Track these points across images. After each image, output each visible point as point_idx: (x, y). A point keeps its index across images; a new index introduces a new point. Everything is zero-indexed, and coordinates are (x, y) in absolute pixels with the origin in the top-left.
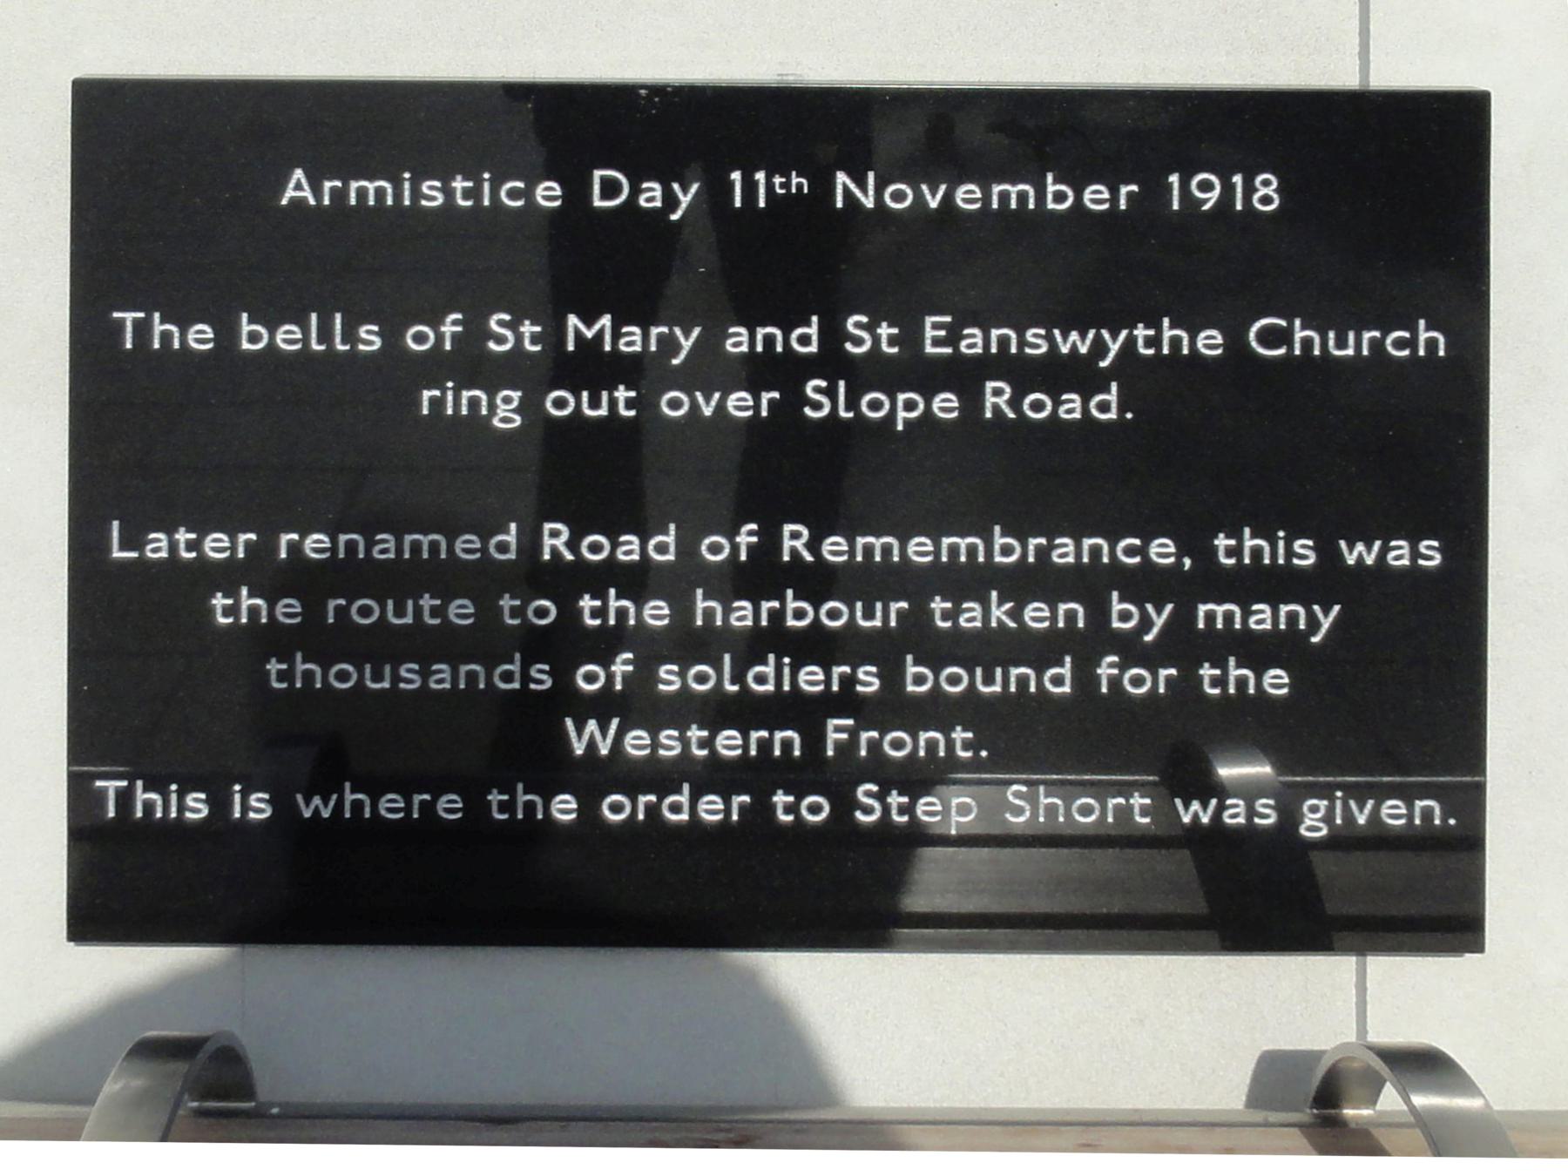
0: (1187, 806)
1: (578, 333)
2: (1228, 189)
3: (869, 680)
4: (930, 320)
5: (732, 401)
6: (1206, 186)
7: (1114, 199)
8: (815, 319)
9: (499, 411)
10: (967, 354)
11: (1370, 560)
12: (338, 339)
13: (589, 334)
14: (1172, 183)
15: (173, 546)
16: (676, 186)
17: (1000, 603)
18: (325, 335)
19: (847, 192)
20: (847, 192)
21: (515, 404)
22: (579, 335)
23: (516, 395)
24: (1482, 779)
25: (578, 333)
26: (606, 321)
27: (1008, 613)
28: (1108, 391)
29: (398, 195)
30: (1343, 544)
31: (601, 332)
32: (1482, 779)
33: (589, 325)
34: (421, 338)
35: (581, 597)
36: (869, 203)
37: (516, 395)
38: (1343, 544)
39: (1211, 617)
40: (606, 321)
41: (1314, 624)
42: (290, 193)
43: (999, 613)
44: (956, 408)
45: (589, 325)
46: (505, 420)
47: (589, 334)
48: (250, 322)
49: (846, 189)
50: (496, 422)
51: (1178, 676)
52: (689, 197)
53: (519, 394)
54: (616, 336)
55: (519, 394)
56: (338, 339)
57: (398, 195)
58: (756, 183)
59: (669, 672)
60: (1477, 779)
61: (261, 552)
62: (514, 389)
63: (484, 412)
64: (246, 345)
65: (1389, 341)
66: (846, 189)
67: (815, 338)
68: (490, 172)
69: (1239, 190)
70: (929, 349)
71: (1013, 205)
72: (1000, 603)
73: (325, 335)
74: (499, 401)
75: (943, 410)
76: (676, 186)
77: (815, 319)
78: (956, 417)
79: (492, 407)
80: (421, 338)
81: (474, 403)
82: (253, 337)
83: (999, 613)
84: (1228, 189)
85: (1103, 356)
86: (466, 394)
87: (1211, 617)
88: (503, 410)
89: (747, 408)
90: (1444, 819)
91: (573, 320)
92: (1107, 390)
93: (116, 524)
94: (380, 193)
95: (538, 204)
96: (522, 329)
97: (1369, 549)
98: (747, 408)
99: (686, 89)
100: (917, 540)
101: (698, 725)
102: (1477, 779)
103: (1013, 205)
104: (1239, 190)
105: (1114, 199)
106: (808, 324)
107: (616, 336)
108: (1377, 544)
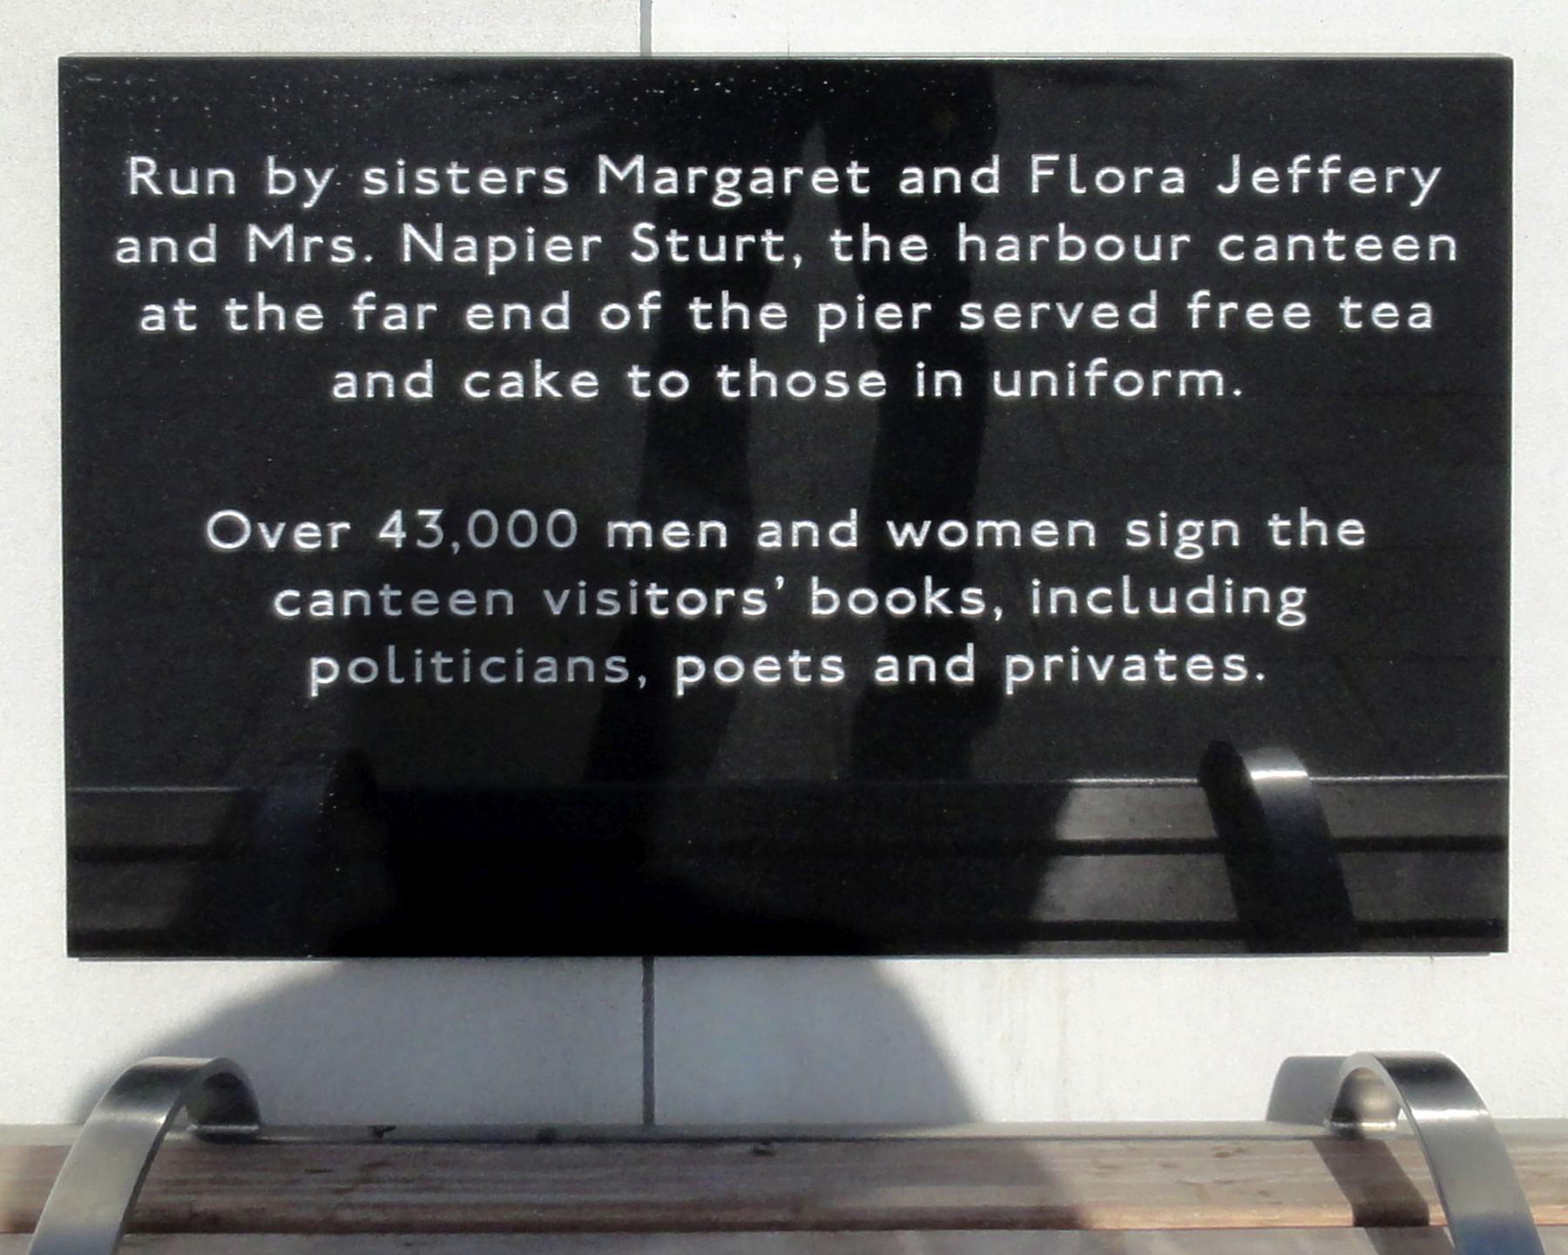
0: (899, 529)
1: (259, 242)
4: (1036, 159)
5: (905, 246)
8: (854, 512)
13: (271, 245)
17: (544, 372)
19: (415, 246)
20: (415, 246)
24: (1505, 777)
25: (259, 242)
26: (638, 162)
27: (551, 382)
28: (827, 332)
31: (633, 175)
32: (1505, 777)
33: (621, 167)
36: (437, 256)
40: (638, 162)
43: (543, 383)
44: (1276, 183)
45: (621, 167)
47: (271, 245)
48: (759, 369)
49: (414, 243)
54: (650, 178)
60: (1498, 777)
61: (361, 542)
63: (1266, 610)
64: (816, 611)
65: (1117, 381)
66: (414, 243)
67: (854, 532)
68: (405, 159)
71: (999, 543)
75: (1263, 185)
77: (854, 512)
78: (1379, 260)
79: (1276, 605)
82: (825, 602)
83: (543, 383)
85: (307, 197)
87: (620, 535)
88: (1287, 608)
90: (1229, 387)
91: (604, 162)
92: (828, 334)
95: (549, 259)
96: (849, 171)
100: (1293, 306)
102: (1498, 777)
103: (999, 543)
106: (847, 518)
107: (650, 178)
108: (927, 525)
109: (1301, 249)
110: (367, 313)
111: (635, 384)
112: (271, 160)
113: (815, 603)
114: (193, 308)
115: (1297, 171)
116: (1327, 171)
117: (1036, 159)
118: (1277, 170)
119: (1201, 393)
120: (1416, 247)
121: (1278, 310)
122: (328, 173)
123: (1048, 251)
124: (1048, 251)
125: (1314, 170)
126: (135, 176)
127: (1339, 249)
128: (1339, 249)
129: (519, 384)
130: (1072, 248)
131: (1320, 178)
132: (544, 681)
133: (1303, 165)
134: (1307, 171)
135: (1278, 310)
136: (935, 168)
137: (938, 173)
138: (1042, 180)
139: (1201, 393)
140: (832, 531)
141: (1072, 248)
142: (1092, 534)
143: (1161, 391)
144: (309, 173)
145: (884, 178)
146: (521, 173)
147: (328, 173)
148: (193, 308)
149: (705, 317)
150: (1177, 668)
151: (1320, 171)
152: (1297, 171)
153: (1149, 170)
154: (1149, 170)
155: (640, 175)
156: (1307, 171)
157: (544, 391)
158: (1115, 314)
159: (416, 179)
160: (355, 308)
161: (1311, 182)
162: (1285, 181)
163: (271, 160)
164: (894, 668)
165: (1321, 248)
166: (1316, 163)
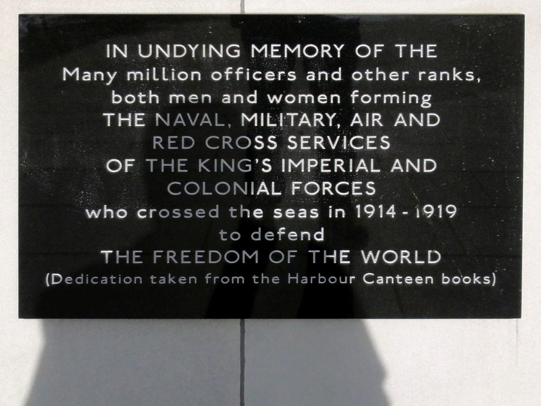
1: (67, 74)
2: (377, 211)
3: (292, 76)
4: (155, 252)
6: (369, 209)
7: (276, 76)
9: (423, 102)
10: (431, 81)
11: (278, 101)
12: (164, 76)
14: (357, 209)
15: (109, 280)
16: (108, 73)
17: (457, 72)
18: (159, 75)
21: (429, 100)
22: (67, 75)
23: (429, 96)
26: (77, 70)
29: (145, 76)
30: (269, 96)
34: (217, 76)
35: (220, 231)
37: (429, 96)
38: (269, 96)
39: (132, 76)
40: (77, 70)
41: (107, 79)
42: (394, 168)
46: (425, 105)
50: (422, 106)
51: (355, 278)
52: (113, 77)
53: (430, 96)
54: (81, 75)
55: (430, 96)
56: (164, 76)
57: (145, 76)
58: (439, 209)
59: (487, 278)
62: (429, 94)
63: (417, 102)
69: (381, 211)
70: (129, 73)
72: (457, 72)
73: (159, 75)
74: (423, 98)
76: (108, 73)
79: (421, 101)
80: (217, 76)
81: (414, 99)
84: (377, 211)
86: (411, 96)
87: (132, 76)
88: (424, 102)
89: (273, 77)
91: (65, 70)
93: (152, 170)
94: (138, 76)
97: (278, 98)
98: (273, 77)
99: (131, 77)
101: (138, 94)
104: (381, 211)
105: (276, 76)
107: (81, 75)
109: (390, 280)
110: (209, 279)
111: (255, 280)
112: (443, 274)
113: (319, 280)
114: (155, 277)
115: (227, 73)
116: (238, 73)
117: (155, 252)
118: (294, 210)
119: (238, 282)
120: (422, 280)
121: (414, 278)
122: (115, 73)
123: (316, 281)
124: (316, 281)
125: (234, 73)
126: (155, 143)
127: (400, 280)
128: (400, 280)
129: (164, 280)
130: (322, 280)
131: (235, 75)
132: (162, 283)
133: (230, 70)
134: (231, 73)
135: (414, 278)
136: (410, 113)
137: (236, 96)
138: (157, 259)
139: (238, 282)
140: (228, 281)
141: (322, 280)
142: (432, 280)
143: (313, 282)
144: (190, 46)
145: (351, 211)
146: (280, 73)
147: (115, 73)
148: (155, 277)
149: (257, 280)
150: (402, 280)
151: (236, 73)
152: (227, 73)
153: (424, 73)
154: (424, 73)
155: (78, 74)
156: (231, 73)
157: (171, 282)
158: (411, 280)
159: (184, 213)
160: (206, 277)
161: (233, 77)
162: (276, 236)
163: (443, 274)
164: (382, 280)
165: (395, 280)
166: (234, 70)
